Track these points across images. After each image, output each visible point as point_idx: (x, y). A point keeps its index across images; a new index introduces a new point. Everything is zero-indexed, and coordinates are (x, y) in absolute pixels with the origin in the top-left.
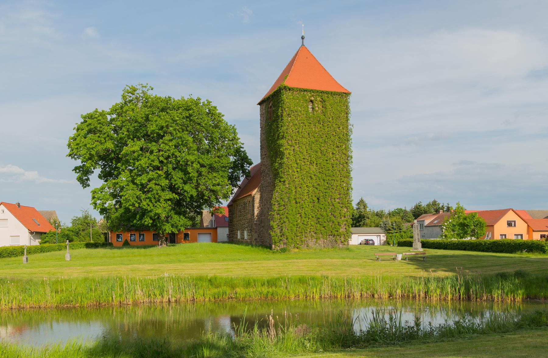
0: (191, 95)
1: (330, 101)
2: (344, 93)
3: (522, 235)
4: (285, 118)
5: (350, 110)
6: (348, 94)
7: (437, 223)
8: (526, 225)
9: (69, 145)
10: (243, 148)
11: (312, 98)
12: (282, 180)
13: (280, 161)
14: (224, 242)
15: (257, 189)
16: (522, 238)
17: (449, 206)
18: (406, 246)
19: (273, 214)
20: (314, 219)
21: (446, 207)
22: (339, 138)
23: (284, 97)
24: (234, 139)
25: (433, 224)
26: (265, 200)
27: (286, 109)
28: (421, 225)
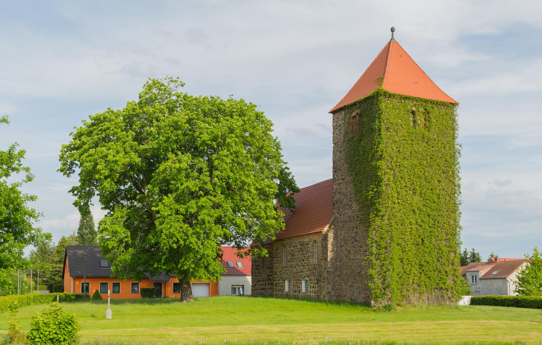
0: (232, 95)
1: (435, 112)
2: (451, 103)
4: (383, 132)
5: (457, 125)
6: (454, 104)
7: (497, 274)
9: (62, 158)
10: (288, 169)
11: (414, 109)
12: (381, 214)
13: (376, 189)
14: (248, 296)
15: (328, 226)
17: (475, 252)
18: (486, 304)
19: (371, 258)
20: (416, 266)
21: (470, 254)
22: (446, 160)
23: (383, 106)
24: (277, 157)
25: (491, 276)
26: (341, 240)
27: (385, 121)
28: (473, 276)
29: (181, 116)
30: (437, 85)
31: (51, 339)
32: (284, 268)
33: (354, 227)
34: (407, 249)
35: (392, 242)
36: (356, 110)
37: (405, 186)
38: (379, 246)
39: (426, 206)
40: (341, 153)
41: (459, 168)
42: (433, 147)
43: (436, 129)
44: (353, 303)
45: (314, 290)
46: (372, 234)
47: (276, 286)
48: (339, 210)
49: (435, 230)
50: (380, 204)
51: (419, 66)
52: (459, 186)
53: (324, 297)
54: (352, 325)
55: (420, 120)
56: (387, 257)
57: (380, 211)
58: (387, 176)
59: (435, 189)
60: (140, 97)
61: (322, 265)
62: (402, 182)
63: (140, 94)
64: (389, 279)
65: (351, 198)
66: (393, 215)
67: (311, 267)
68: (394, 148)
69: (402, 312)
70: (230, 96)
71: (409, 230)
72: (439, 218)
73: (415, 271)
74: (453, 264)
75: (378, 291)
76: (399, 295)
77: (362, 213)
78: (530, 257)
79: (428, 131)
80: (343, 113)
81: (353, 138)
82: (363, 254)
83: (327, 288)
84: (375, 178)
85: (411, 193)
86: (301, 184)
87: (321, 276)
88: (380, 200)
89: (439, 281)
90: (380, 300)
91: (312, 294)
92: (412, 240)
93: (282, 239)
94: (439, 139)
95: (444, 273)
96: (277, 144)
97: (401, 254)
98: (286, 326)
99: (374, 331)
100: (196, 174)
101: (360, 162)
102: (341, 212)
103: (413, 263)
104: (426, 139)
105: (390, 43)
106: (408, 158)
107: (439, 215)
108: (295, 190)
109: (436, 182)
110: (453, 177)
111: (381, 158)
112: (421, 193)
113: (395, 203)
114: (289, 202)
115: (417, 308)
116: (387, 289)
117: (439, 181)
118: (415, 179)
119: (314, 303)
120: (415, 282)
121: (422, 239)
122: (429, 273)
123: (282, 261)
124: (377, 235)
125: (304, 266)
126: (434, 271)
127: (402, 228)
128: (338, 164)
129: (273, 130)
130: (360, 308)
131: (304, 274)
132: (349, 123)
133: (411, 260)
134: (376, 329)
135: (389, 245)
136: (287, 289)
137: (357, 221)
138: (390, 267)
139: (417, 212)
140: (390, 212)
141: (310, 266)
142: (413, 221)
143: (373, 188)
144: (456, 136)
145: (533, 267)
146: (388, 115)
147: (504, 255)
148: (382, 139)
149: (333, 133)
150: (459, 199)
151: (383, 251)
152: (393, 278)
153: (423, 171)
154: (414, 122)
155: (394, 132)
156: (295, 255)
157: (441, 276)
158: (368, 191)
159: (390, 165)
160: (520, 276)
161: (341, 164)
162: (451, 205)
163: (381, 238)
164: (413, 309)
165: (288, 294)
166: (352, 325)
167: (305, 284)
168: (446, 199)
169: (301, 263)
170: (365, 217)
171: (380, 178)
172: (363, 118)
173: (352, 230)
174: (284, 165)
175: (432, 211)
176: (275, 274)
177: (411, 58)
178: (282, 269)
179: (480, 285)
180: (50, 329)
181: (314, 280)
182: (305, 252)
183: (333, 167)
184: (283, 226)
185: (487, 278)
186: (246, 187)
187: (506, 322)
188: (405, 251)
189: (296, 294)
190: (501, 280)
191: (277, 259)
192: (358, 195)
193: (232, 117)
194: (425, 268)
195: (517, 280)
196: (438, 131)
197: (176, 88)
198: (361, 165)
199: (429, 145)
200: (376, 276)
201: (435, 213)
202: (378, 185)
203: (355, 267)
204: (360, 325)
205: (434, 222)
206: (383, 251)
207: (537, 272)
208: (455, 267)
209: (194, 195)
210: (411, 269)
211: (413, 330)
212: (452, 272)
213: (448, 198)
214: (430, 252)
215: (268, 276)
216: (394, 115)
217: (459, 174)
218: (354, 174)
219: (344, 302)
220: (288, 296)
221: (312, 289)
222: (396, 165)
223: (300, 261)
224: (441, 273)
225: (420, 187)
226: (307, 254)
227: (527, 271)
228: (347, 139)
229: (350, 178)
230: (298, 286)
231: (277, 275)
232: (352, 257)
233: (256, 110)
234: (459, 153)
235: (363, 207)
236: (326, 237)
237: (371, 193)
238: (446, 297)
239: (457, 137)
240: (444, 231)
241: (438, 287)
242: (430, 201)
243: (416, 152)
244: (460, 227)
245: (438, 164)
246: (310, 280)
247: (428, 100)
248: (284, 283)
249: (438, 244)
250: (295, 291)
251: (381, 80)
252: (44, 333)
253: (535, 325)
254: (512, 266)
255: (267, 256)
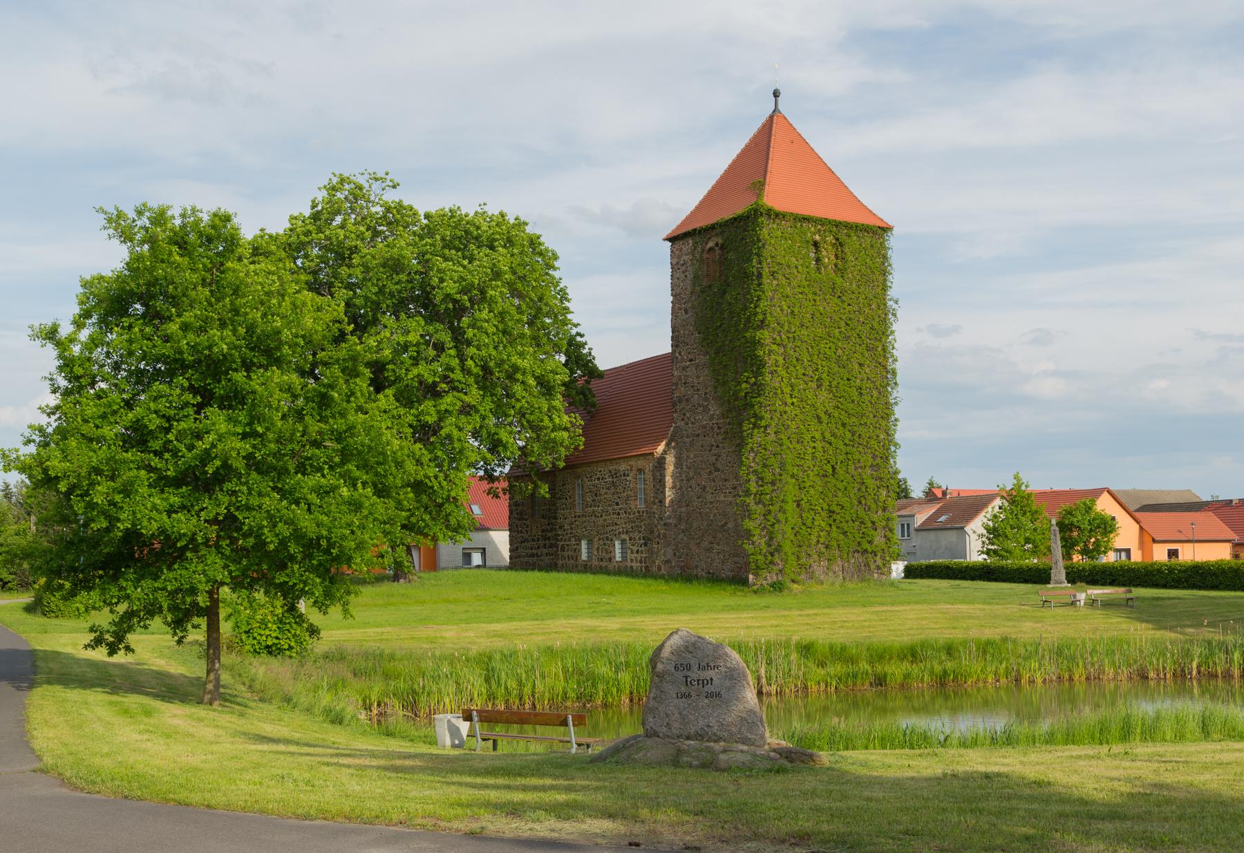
0: (485, 204)
1: (853, 242)
2: (879, 227)
3: (1128, 551)
4: (766, 280)
5: (890, 265)
6: (885, 229)
7: (947, 522)
8: (1137, 526)
10: (582, 336)
11: (817, 237)
12: (763, 423)
16: (1129, 557)
25: (936, 525)
26: (689, 468)
28: (903, 526)
29: (404, 246)
30: (855, 194)
31: (268, 647)
32: (579, 517)
33: (713, 445)
34: (807, 484)
35: (783, 473)
36: (714, 238)
37: (804, 374)
38: (762, 479)
39: (838, 408)
40: (686, 312)
41: (893, 342)
42: (849, 305)
43: (855, 273)
44: (714, 579)
45: (639, 556)
46: (748, 459)
47: (563, 549)
48: (684, 414)
49: (854, 449)
50: (761, 407)
51: (829, 165)
52: (894, 373)
53: (659, 568)
54: (735, 616)
55: (828, 257)
56: (774, 499)
57: (761, 418)
58: (773, 357)
59: (853, 379)
60: (313, 207)
61: (654, 513)
62: (798, 368)
63: (313, 201)
64: (779, 537)
65: (706, 394)
66: (783, 425)
67: (632, 516)
68: (785, 307)
69: (802, 592)
70: (480, 205)
71: (810, 451)
72: (861, 428)
73: (821, 522)
74: (884, 510)
75: (760, 557)
76: (795, 563)
77: (728, 421)
78: (1008, 489)
79: (842, 276)
80: (691, 242)
81: (710, 287)
82: (730, 493)
83: (664, 553)
84: (752, 359)
85: (814, 385)
86: (604, 362)
87: (652, 532)
88: (760, 399)
89: (862, 538)
90: (764, 573)
91: (634, 565)
92: (815, 469)
93: (574, 465)
94: (860, 291)
95: (870, 525)
96: (560, 291)
97: (797, 492)
98: (627, 620)
99: (772, 626)
100: (432, 353)
101: (724, 331)
102: (689, 419)
103: (817, 507)
104: (839, 291)
105: (771, 117)
106: (809, 324)
107: (861, 424)
108: (592, 372)
109: (857, 366)
110: (884, 356)
111: (762, 325)
112: (830, 386)
113: (786, 404)
114: (585, 396)
115: (825, 586)
116: (776, 553)
117: (861, 365)
118: (819, 362)
119: (643, 581)
120: (822, 540)
121: (833, 466)
122: (844, 524)
123: (574, 505)
124: (757, 460)
125: (619, 514)
126: (853, 521)
127: (798, 447)
128: (682, 332)
129: (559, 268)
130: (729, 588)
131: (619, 529)
132: (702, 260)
133: (814, 502)
134: (774, 622)
135: (778, 477)
136: (584, 556)
137: (717, 434)
138: (781, 516)
139: (824, 418)
140: (779, 419)
141: (630, 514)
142: (818, 436)
143: (748, 378)
144: (889, 284)
145: (1013, 507)
146: (773, 250)
147: (958, 481)
148: (764, 292)
149: (672, 276)
150: (895, 394)
151: (768, 488)
152: (785, 534)
153: (833, 347)
154: (818, 260)
155: (784, 278)
156: (600, 495)
157: (864, 530)
158: (739, 383)
159: (778, 338)
160: (991, 524)
161: (687, 332)
162: (881, 406)
163: (765, 466)
164: (819, 588)
165: (586, 565)
166: (735, 616)
167: (586, 547)
168: (872, 396)
169: (613, 509)
170: (732, 428)
171: (760, 361)
172: (728, 252)
173: (709, 451)
174: (574, 328)
175: (849, 418)
176: (560, 528)
177: (809, 145)
178: (574, 519)
179: (917, 540)
180: (267, 632)
181: (640, 539)
182: (620, 489)
183: (672, 337)
184: (581, 443)
185: (929, 527)
186: (519, 376)
187: (982, 606)
188: (805, 488)
189: (604, 564)
190: (955, 532)
191: (564, 501)
192: (720, 389)
193: (492, 248)
194: (838, 517)
195: (985, 532)
196: (859, 277)
197: (382, 192)
198: (726, 336)
199: (843, 301)
200: (757, 532)
201: (854, 419)
202: (756, 372)
203: (715, 515)
204: (746, 616)
205: (853, 435)
206: (768, 488)
207: (1019, 516)
208: (887, 514)
209: (432, 391)
210: (813, 519)
211: (836, 623)
212: (884, 523)
213: (875, 393)
214: (846, 489)
215: (543, 531)
216: (784, 250)
217: (894, 351)
218: (712, 351)
219: (697, 578)
220: (586, 568)
221: (635, 555)
222: (788, 338)
223: (610, 505)
224: (865, 524)
225: (828, 375)
226: (624, 492)
227: (1001, 516)
228: (698, 289)
229: (702, 359)
230: (606, 550)
231: (564, 530)
232: (709, 498)
233: (527, 231)
234: (894, 315)
235: (729, 411)
236: (661, 463)
237: (744, 385)
238: (873, 567)
239: (890, 287)
240: (869, 451)
241: (859, 549)
242: (846, 400)
243: (821, 314)
244: (896, 445)
245: (858, 335)
246: (630, 540)
247: (840, 223)
248: (579, 544)
249: (860, 475)
250: (602, 560)
251: (759, 187)
252: (258, 637)
253: (1028, 611)
254: (973, 505)
255: (547, 496)
